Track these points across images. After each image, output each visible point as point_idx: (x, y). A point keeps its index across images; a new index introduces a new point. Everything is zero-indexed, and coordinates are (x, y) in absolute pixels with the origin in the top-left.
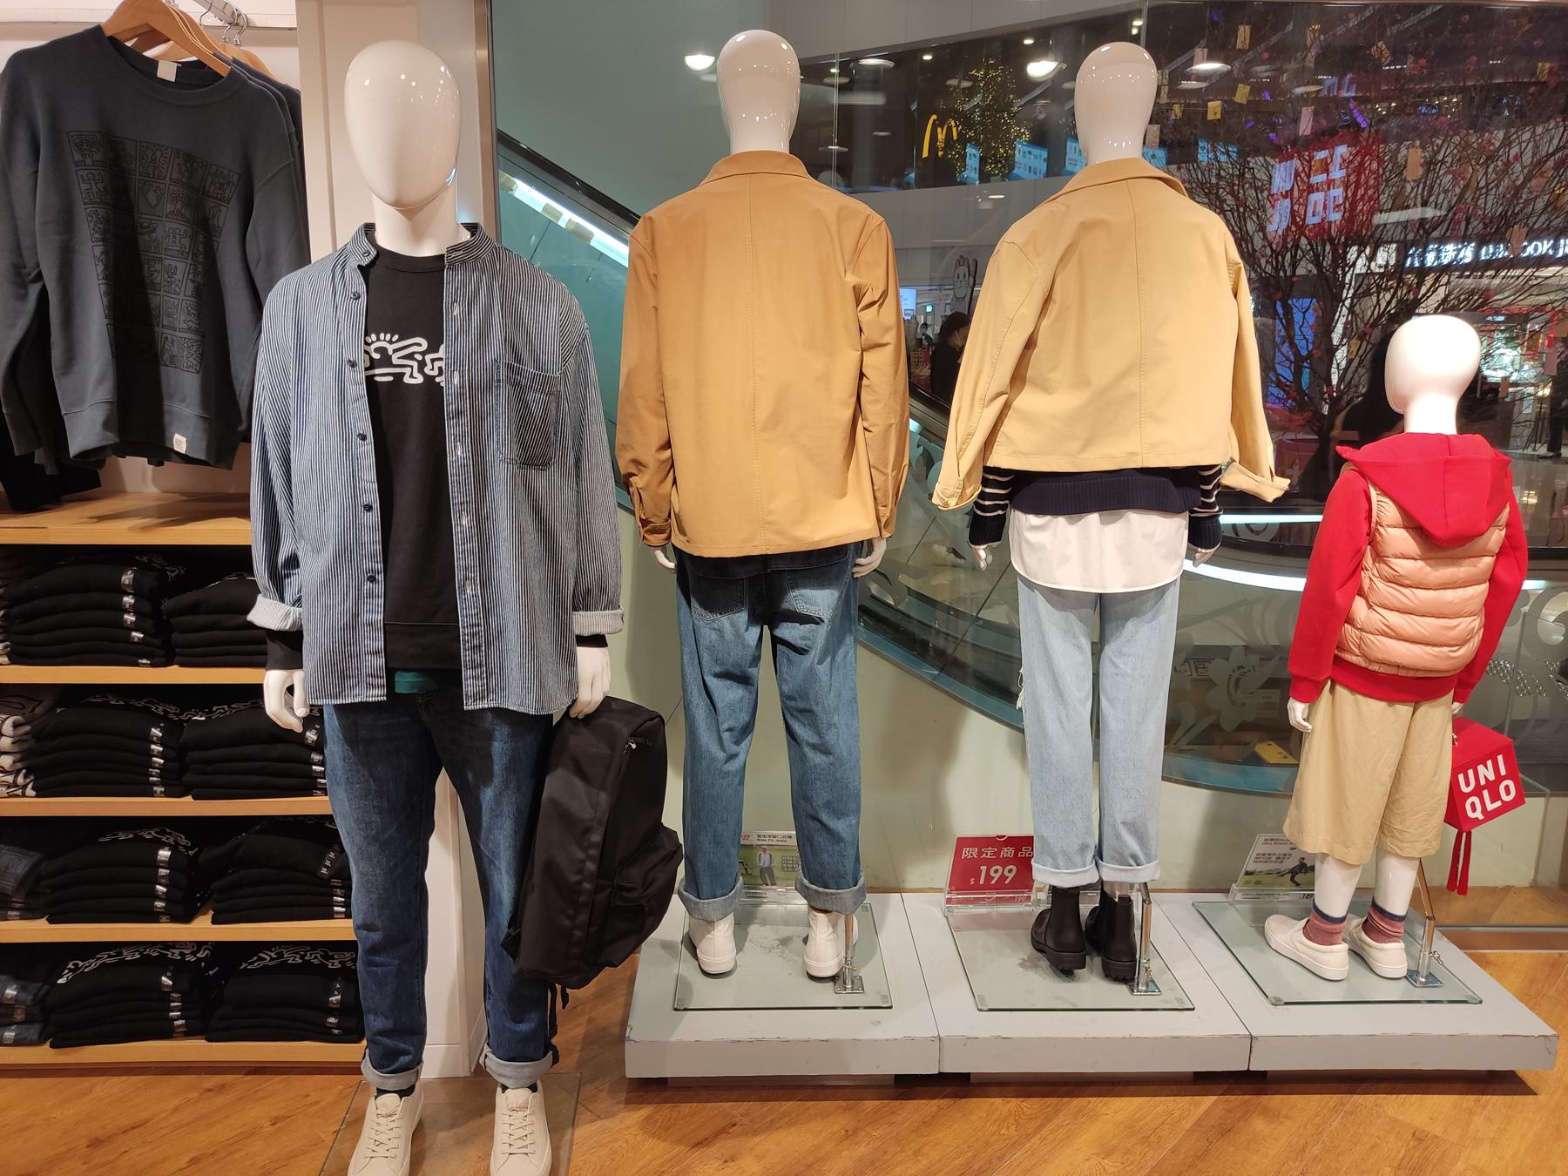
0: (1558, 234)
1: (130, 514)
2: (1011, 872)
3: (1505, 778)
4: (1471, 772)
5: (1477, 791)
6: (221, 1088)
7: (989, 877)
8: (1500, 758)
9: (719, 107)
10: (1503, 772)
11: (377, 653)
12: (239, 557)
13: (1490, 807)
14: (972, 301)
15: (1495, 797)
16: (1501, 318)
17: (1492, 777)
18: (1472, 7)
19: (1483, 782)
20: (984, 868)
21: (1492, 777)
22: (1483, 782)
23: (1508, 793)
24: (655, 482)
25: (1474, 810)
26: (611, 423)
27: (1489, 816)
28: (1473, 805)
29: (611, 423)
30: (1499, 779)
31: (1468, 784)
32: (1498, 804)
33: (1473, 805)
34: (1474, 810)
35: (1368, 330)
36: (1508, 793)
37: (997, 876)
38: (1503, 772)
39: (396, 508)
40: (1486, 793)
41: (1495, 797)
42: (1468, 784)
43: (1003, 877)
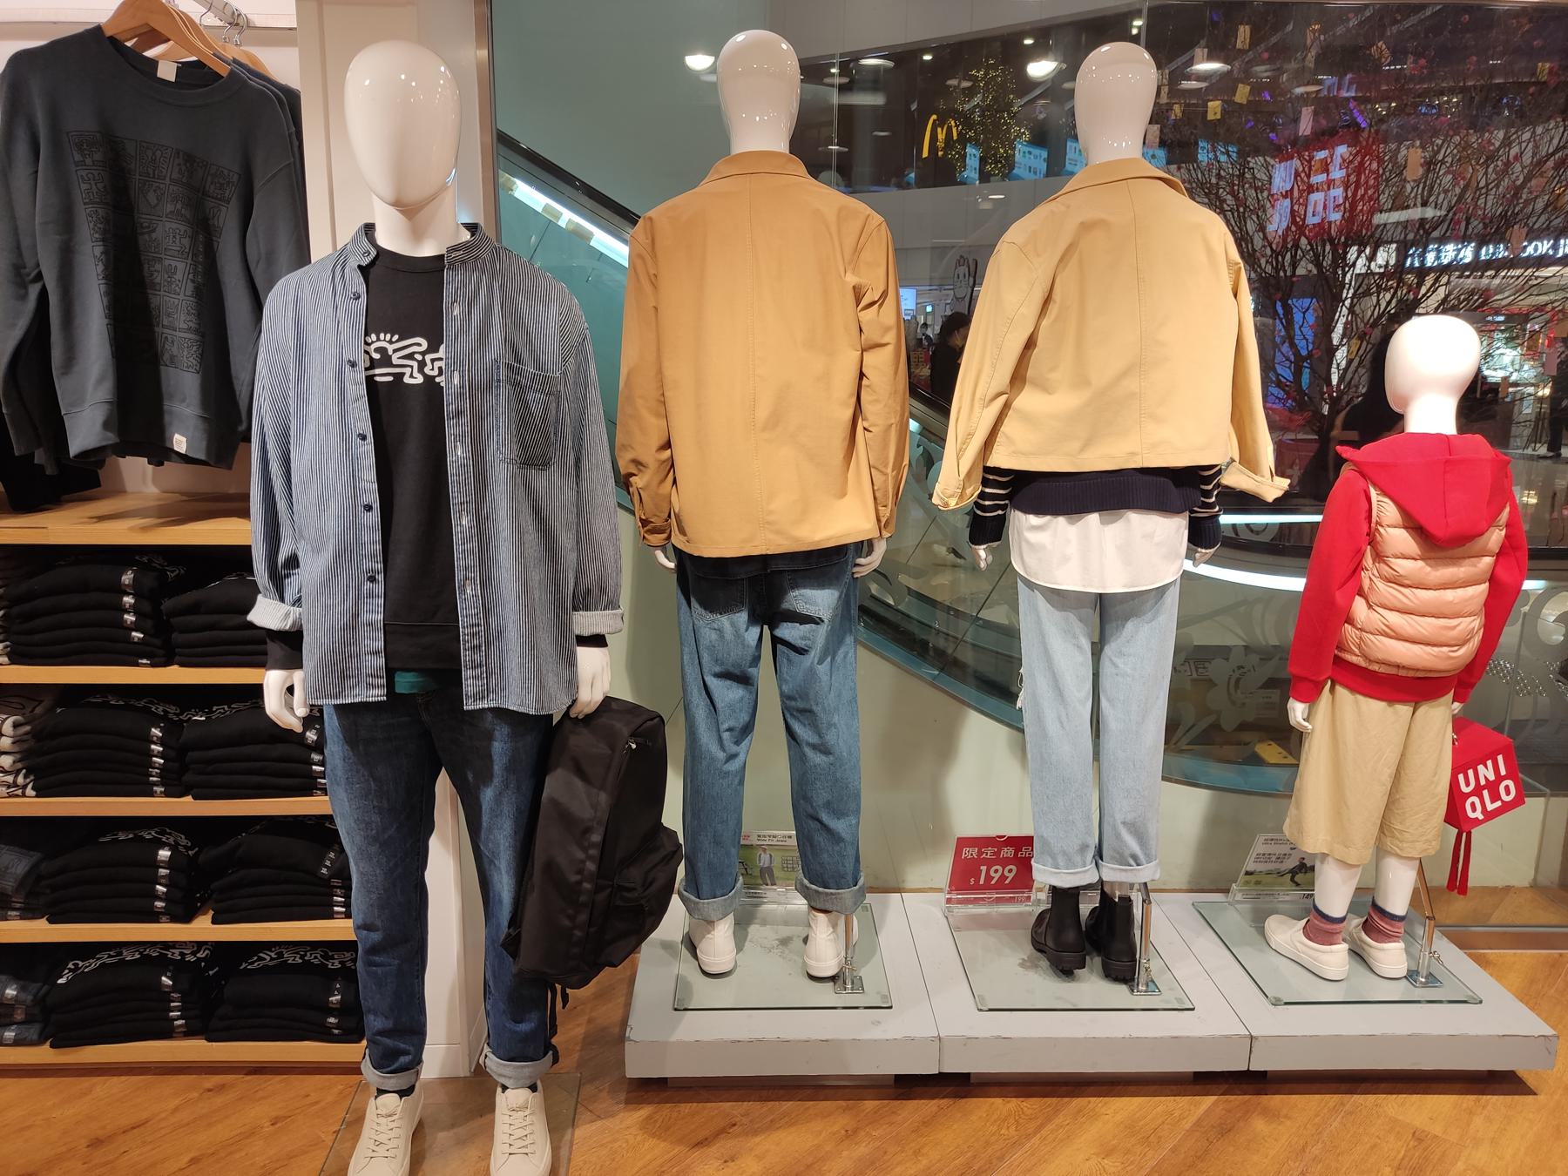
0: (1558, 234)
1: (130, 514)
2: (1011, 872)
3: (1505, 778)
4: (1471, 772)
5: (1477, 791)
6: (221, 1088)
7: (989, 877)
8: (1500, 758)
9: (719, 107)
10: (1503, 772)
11: (377, 653)
12: (239, 557)
13: (1490, 807)
14: (972, 301)
15: (1495, 797)
16: (1501, 318)
17: (1492, 777)
18: (1472, 7)
19: (1483, 782)
20: (984, 868)
21: (1492, 777)
22: (1483, 782)
23: (1508, 793)
24: (655, 482)
25: (1474, 810)
26: (611, 423)
27: (1489, 816)
28: (1473, 805)
29: (611, 423)
30: (1499, 779)
31: (1468, 784)
32: (1498, 804)
33: (1473, 805)
34: (1474, 810)
35: (1368, 330)
36: (1508, 793)
37: (997, 876)
38: (1503, 772)
39: (396, 508)
40: (1486, 793)
41: (1495, 797)
42: (1468, 784)
43: (1003, 877)
